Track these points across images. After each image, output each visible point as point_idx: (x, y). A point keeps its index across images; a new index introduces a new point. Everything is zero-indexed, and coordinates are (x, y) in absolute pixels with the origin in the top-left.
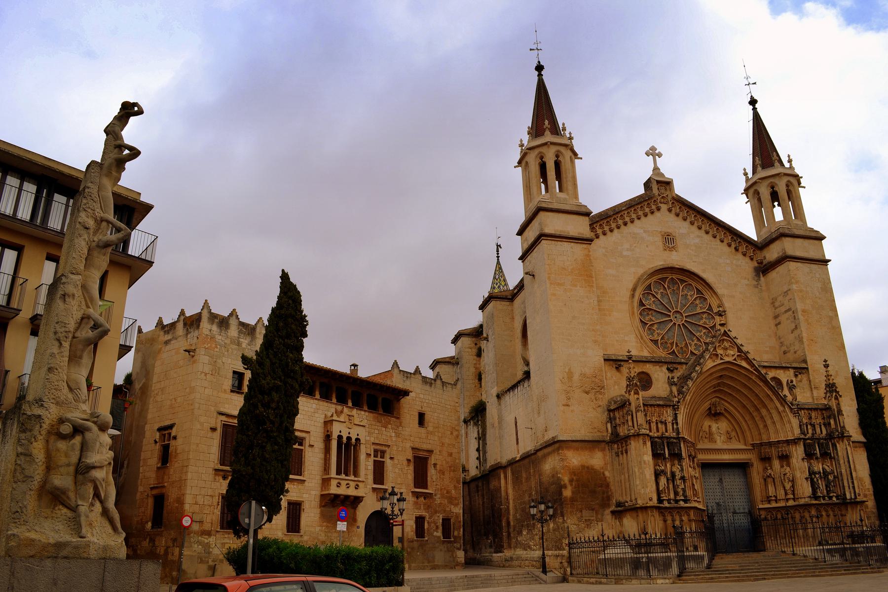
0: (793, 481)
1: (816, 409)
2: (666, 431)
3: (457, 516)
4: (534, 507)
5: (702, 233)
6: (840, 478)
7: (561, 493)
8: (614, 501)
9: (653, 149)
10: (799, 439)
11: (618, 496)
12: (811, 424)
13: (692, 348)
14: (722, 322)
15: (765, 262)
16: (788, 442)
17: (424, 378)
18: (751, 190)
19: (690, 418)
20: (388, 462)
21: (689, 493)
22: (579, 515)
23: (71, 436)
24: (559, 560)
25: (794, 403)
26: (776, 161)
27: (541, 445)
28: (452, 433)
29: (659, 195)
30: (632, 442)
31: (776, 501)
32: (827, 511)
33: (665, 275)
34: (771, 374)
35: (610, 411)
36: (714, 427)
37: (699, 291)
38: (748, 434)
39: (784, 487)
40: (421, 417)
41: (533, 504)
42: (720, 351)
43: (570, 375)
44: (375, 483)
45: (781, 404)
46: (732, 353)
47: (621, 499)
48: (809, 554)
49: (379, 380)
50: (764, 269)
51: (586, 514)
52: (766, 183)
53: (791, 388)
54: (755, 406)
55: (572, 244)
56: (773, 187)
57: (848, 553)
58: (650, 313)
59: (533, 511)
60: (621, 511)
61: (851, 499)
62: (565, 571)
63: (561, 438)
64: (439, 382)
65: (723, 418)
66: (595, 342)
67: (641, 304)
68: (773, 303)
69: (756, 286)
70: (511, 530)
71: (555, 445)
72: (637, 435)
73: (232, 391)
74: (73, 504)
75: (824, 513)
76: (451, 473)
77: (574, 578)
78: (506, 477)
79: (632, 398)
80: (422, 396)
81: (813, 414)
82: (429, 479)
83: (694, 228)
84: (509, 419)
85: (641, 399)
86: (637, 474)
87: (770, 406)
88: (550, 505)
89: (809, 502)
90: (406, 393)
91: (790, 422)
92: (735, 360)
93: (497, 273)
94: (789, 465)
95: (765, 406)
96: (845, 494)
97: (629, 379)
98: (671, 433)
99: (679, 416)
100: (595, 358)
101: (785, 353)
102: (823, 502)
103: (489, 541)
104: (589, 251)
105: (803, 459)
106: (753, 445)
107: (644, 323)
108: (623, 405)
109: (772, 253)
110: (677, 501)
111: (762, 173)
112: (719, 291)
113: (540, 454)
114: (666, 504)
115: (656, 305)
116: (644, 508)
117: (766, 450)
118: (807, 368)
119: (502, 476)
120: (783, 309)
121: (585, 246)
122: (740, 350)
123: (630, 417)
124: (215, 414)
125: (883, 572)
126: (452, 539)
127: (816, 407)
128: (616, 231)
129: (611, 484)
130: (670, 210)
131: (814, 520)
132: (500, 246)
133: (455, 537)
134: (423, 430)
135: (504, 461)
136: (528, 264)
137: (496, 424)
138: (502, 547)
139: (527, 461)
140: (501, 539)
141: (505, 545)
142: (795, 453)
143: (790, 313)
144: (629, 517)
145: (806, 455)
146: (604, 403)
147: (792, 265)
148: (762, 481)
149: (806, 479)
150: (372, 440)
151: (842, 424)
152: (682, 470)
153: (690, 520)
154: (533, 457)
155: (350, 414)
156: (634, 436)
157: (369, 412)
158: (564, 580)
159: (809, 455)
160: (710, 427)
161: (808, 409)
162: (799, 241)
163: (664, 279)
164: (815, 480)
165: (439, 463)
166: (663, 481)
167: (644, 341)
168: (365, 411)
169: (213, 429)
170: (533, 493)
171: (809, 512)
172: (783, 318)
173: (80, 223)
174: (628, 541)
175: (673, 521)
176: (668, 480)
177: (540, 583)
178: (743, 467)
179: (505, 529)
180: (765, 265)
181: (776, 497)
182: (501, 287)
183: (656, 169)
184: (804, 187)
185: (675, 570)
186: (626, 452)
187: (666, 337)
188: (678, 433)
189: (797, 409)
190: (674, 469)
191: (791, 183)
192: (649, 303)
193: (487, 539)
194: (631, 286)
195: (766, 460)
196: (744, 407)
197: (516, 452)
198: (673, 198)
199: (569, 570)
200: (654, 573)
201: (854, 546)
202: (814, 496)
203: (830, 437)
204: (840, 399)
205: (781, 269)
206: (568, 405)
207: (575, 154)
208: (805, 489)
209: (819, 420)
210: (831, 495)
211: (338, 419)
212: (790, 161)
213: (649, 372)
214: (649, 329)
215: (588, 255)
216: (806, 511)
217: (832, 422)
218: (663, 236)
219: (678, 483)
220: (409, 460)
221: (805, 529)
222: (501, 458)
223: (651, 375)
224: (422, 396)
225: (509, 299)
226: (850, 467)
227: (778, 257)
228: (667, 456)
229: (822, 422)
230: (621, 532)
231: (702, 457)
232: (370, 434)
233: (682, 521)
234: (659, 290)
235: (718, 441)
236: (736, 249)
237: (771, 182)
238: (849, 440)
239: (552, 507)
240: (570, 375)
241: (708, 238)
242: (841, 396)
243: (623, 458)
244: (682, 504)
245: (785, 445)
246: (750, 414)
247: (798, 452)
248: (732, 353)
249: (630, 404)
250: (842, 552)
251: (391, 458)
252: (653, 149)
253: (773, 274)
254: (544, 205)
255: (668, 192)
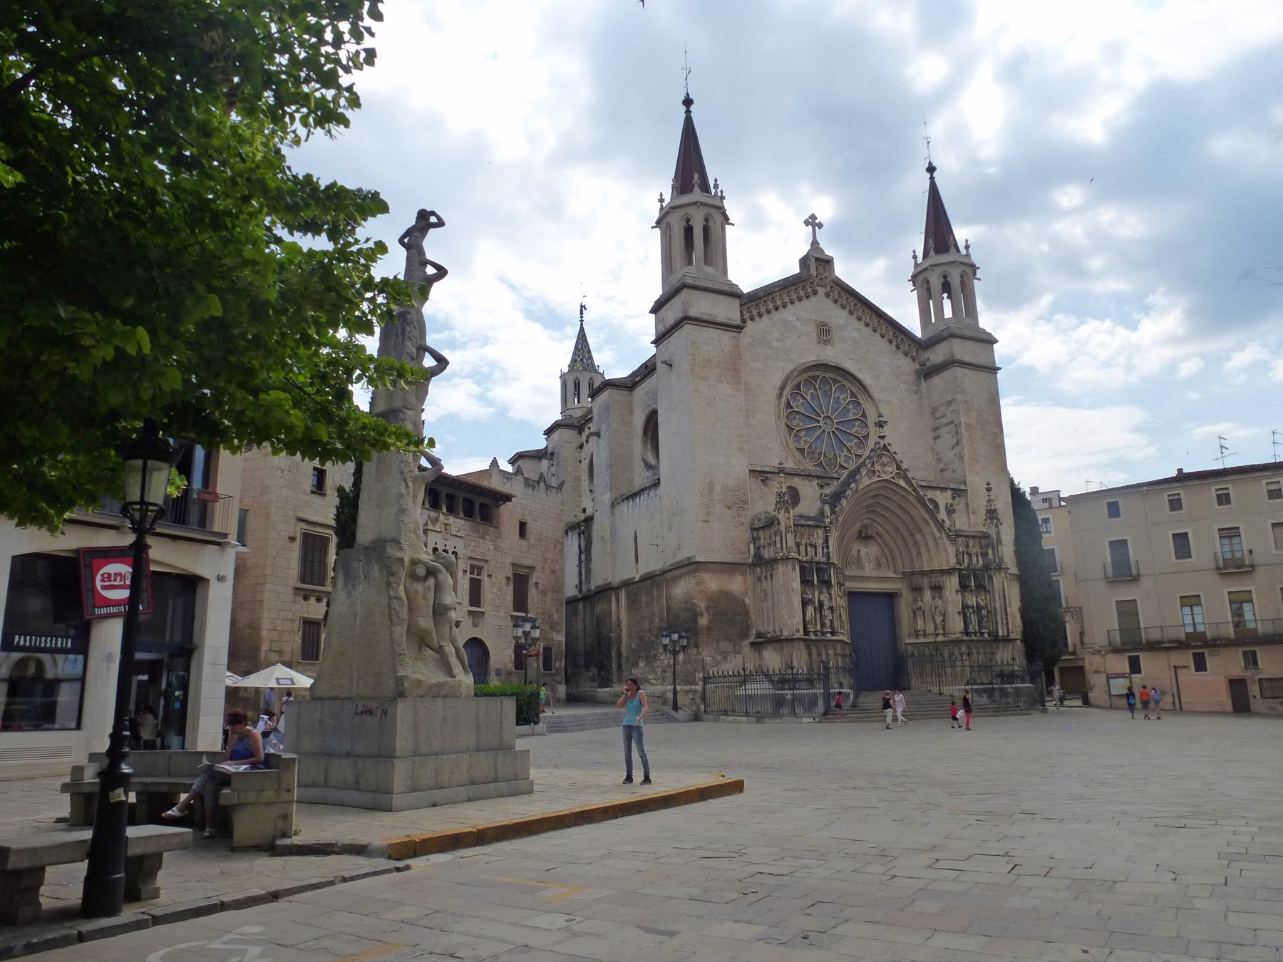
0: (944, 615)
1: (973, 537)
2: (816, 556)
3: (559, 643)
4: (666, 636)
5: (861, 325)
6: (994, 613)
7: (695, 621)
8: (754, 632)
9: (813, 217)
10: (955, 569)
11: (760, 625)
12: (967, 553)
13: (841, 460)
14: (882, 434)
15: (928, 364)
16: (942, 572)
17: (526, 479)
18: (920, 279)
19: (841, 538)
20: (486, 582)
21: (836, 624)
22: (715, 645)
23: (426, 578)
24: (691, 696)
25: (952, 529)
26: (952, 246)
27: (671, 565)
28: (555, 547)
29: (817, 276)
30: (780, 567)
31: (924, 636)
32: (977, 648)
33: (817, 373)
34: (930, 494)
35: (753, 529)
36: (864, 551)
37: (853, 395)
38: (899, 562)
39: (934, 621)
40: (523, 526)
41: (665, 633)
42: (877, 468)
43: (711, 486)
44: (471, 606)
45: (939, 530)
46: (890, 469)
47: (762, 630)
48: (956, 694)
49: (471, 480)
50: (928, 372)
51: (724, 645)
52: (939, 270)
53: (950, 511)
54: (909, 530)
55: (720, 331)
56: (945, 277)
57: (997, 694)
58: (798, 417)
59: (666, 641)
60: (762, 642)
61: (1004, 636)
62: (698, 708)
63: (699, 559)
64: (542, 484)
65: (872, 541)
66: (741, 449)
67: (789, 406)
68: (933, 413)
69: (916, 392)
70: (623, 661)
71: (691, 566)
72: (786, 559)
73: (313, 492)
74: (436, 645)
75: (974, 651)
76: (554, 594)
77: (710, 716)
78: (618, 600)
79: (782, 516)
80: (523, 501)
81: (971, 542)
82: (529, 600)
83: (853, 319)
84: (626, 533)
85: (791, 518)
86: (784, 602)
87: (926, 530)
88: (684, 634)
89: (960, 639)
90: (508, 498)
91: (945, 550)
92: (893, 478)
93: (580, 341)
94: (941, 597)
95: (921, 531)
96: (997, 631)
97: (780, 495)
98: (820, 558)
99: (830, 538)
100: (740, 467)
101: (942, 471)
102: (974, 638)
103: (591, 674)
104: (738, 341)
105: (957, 591)
106: (904, 573)
107: (790, 429)
108: (771, 523)
109: (937, 355)
110: (824, 634)
111: (935, 259)
112: (876, 396)
113: (669, 575)
114: (812, 637)
115: (805, 408)
116: (790, 640)
117: (917, 580)
118: (966, 490)
119: (613, 599)
120: (944, 421)
121: (734, 334)
122: (899, 467)
123: (778, 539)
124: (294, 520)
125: (1031, 714)
126: (553, 672)
127: (975, 534)
128: (765, 316)
129: (751, 612)
130: (827, 295)
131: (964, 657)
132: (584, 307)
133: (556, 669)
134: (523, 543)
135: (616, 581)
136: (664, 350)
137: (608, 537)
138: (611, 680)
139: (648, 583)
140: (609, 672)
141: (615, 679)
142: (948, 584)
143: (952, 426)
144: (770, 649)
145: (961, 587)
146: (747, 520)
147: (960, 371)
148: (912, 615)
149: (959, 613)
150: (469, 553)
151: (1000, 555)
152: (831, 599)
153: (836, 655)
154: (658, 578)
155: (446, 522)
156: (782, 559)
157: (466, 520)
158: (696, 718)
159: (964, 587)
160: (858, 551)
161: (966, 536)
162: (969, 344)
163: (815, 378)
164: (968, 614)
165: (541, 582)
166: (810, 611)
167: (790, 450)
168: (461, 518)
169: (292, 539)
170: (657, 620)
171: (960, 649)
172: (943, 431)
173: (407, 353)
174: (767, 675)
175: (819, 655)
176: (815, 609)
177: (672, 722)
178: (891, 597)
179: (615, 660)
180: (928, 368)
181: (924, 631)
182: (585, 361)
183: (815, 243)
184: (979, 279)
185: (821, 708)
186: (772, 577)
187: (814, 446)
188: (828, 558)
189: (955, 536)
190: (822, 598)
191: (966, 274)
192: (798, 405)
193: (588, 670)
194: (778, 384)
195: (917, 590)
196: (897, 530)
197: (635, 573)
198: (833, 281)
199: (702, 707)
200: (799, 710)
201: (1003, 686)
202: (967, 633)
203: (987, 567)
204: (1000, 527)
205: (946, 375)
206: (707, 522)
207: (727, 219)
208: (957, 625)
209: (977, 550)
210: (984, 631)
211: (433, 528)
212: (967, 247)
213: (798, 487)
214: (796, 436)
215: (737, 346)
216: (956, 647)
217: (990, 552)
218: (817, 325)
219: (826, 614)
220: (508, 578)
221: (953, 667)
222: (613, 577)
223: (800, 492)
224: (523, 501)
225: (628, 387)
226: (1005, 602)
227: (945, 361)
228: (815, 583)
229: (979, 551)
230: (760, 666)
231: (851, 585)
232: (466, 546)
233: (827, 655)
234: (809, 390)
235: (867, 568)
236: (898, 347)
237: (944, 271)
238: (1006, 573)
239: (685, 637)
240: (711, 486)
241: (868, 331)
242: (1001, 524)
243: (766, 584)
244: (829, 635)
245: (938, 575)
246: (904, 539)
247: (952, 583)
248: (890, 469)
249: (779, 523)
250: (990, 692)
251: (489, 576)
252: (813, 217)
253: (937, 380)
254: (690, 281)
255: (827, 274)
